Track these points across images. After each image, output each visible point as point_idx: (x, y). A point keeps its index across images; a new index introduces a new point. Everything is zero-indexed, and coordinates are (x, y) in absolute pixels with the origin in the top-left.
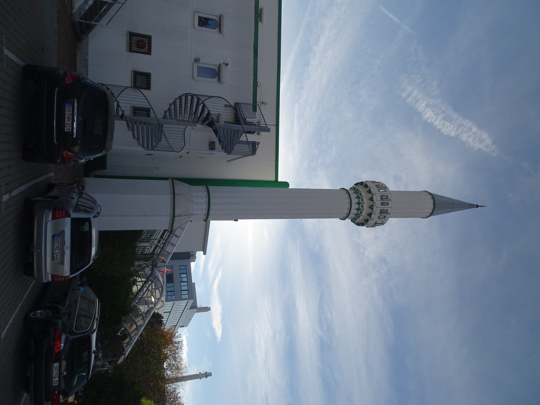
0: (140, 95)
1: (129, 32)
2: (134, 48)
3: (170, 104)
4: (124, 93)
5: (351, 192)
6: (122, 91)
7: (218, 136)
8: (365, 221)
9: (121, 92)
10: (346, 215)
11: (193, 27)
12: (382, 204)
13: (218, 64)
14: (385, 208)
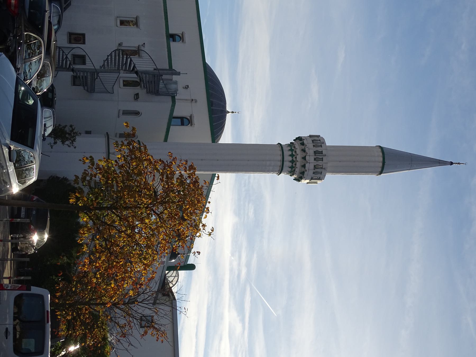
0: (81, 51)
1: (69, 33)
2: (73, 41)
3: (107, 55)
8: (301, 173)
9: (69, 53)
10: (281, 162)
11: (116, 25)
12: (315, 159)
13: (138, 46)
14: (319, 149)
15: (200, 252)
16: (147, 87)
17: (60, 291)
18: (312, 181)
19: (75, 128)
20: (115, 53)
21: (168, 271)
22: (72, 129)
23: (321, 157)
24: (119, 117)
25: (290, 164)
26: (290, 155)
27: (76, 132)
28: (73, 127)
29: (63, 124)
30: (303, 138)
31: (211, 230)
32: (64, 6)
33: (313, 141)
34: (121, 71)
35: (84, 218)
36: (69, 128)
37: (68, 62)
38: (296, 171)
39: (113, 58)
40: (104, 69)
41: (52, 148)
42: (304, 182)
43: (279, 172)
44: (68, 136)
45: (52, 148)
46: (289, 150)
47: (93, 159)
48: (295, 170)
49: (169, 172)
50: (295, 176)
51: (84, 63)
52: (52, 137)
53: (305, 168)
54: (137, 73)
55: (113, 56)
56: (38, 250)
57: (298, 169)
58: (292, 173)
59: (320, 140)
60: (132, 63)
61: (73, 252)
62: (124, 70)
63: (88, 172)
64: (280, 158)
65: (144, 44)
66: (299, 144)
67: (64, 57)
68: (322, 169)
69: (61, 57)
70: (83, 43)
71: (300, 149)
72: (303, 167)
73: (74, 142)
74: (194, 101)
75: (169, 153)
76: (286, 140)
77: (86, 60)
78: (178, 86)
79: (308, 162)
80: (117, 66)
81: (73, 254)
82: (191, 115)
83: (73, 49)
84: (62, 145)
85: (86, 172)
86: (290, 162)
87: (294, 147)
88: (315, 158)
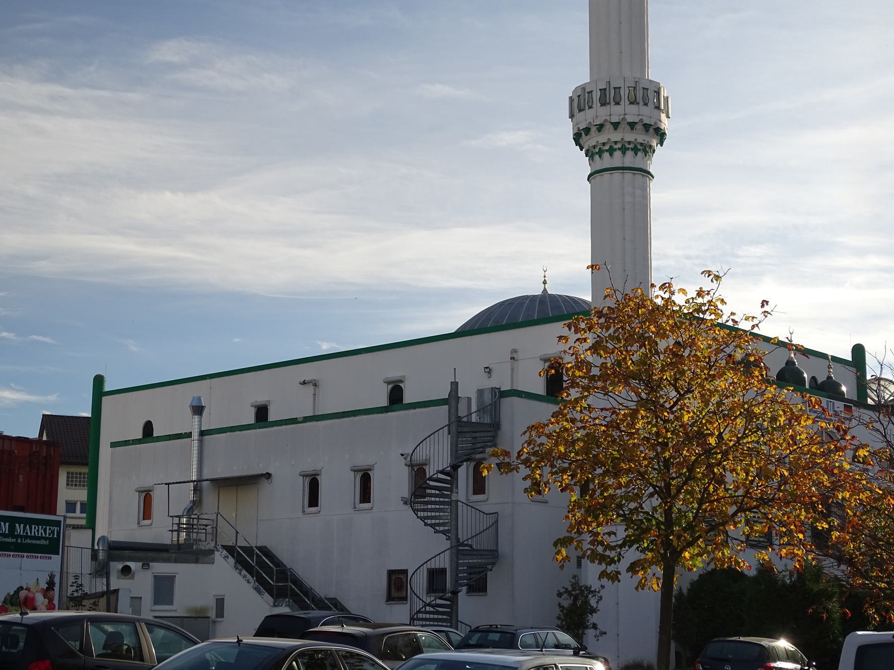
1: (387, 601)
4: (418, 593)
5: (600, 164)
6: (419, 598)
7: (461, 464)
8: (647, 131)
9: (420, 599)
12: (617, 103)
14: (596, 95)
15: (764, 301)
16: (482, 446)
17: (886, 613)
18: (662, 108)
19: (564, 588)
20: (418, 510)
21: (868, 399)
22: (565, 592)
23: (613, 92)
24: (546, 502)
25: (630, 153)
26: (611, 155)
27: (571, 585)
28: (562, 590)
29: (557, 611)
30: (576, 131)
31: (708, 277)
32: (334, 611)
33: (580, 110)
34: (454, 498)
35: (685, 557)
36: (564, 599)
37: (439, 602)
38: (643, 142)
39: (429, 514)
40: (450, 531)
41: (605, 633)
42: (666, 124)
43: (647, 176)
44: (580, 601)
45: (605, 633)
46: (600, 157)
47: (559, 539)
48: (641, 144)
49: (576, 372)
50: (654, 143)
51: (443, 571)
52: (583, 633)
53: (636, 123)
54: (455, 467)
55: (426, 515)
56: (810, 660)
57: (640, 137)
58: (647, 150)
59: (578, 96)
60: (436, 476)
61: (816, 589)
62: (452, 492)
63: (588, 549)
64: (617, 175)
65: (402, 455)
66: (588, 137)
67: (432, 609)
68: (638, 88)
69: (432, 616)
70: (405, 575)
71: (598, 136)
72: (634, 128)
73: (593, 589)
74: (515, 355)
75: (540, 375)
76: (582, 164)
77: (436, 567)
78: (486, 387)
79: (623, 117)
80: (446, 507)
81: (821, 590)
82: (541, 360)
83: (413, 592)
84: (598, 612)
85: (587, 554)
86: (624, 153)
87: (594, 148)
88: (614, 103)
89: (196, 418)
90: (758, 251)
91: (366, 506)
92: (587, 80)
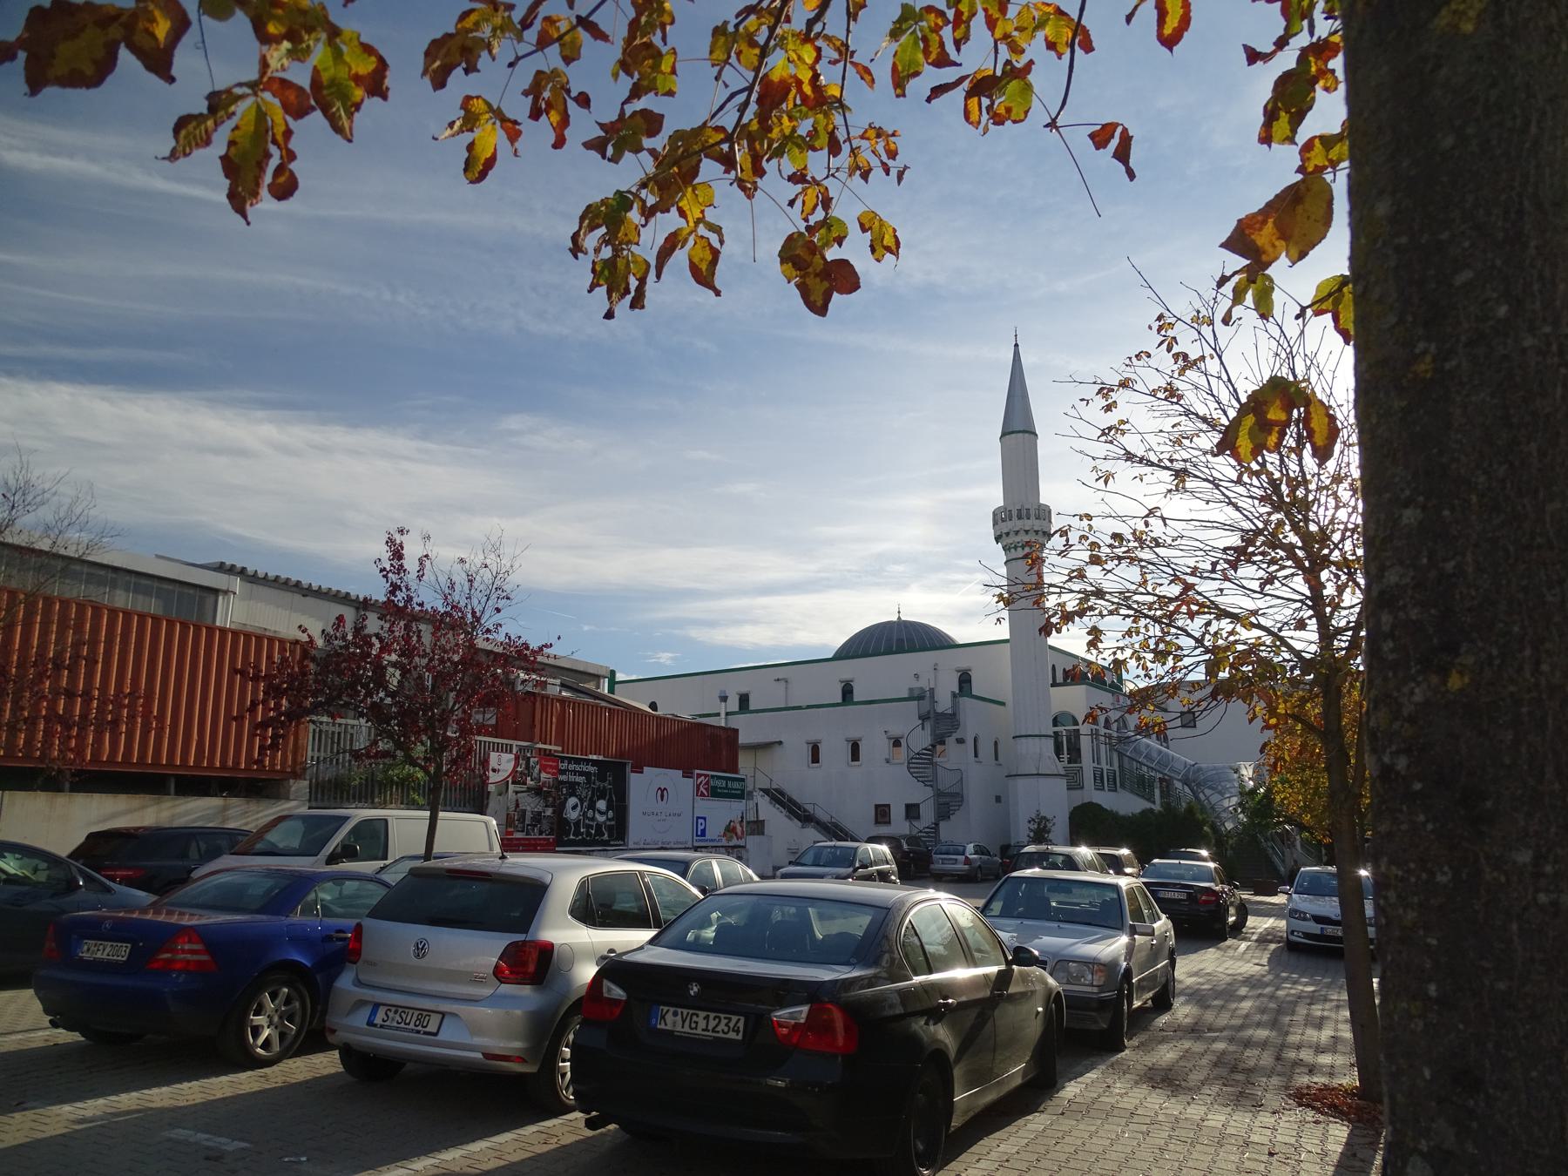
2: (887, 820)
14: (1015, 513)
89: (723, 704)
90: (900, 568)
91: (856, 763)
92: (1001, 504)
